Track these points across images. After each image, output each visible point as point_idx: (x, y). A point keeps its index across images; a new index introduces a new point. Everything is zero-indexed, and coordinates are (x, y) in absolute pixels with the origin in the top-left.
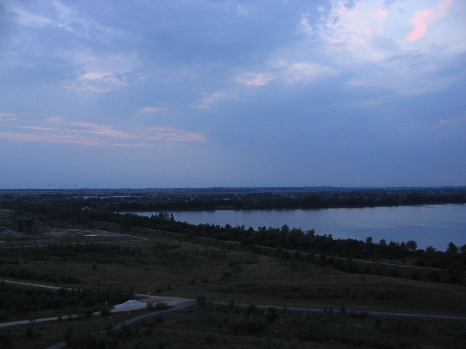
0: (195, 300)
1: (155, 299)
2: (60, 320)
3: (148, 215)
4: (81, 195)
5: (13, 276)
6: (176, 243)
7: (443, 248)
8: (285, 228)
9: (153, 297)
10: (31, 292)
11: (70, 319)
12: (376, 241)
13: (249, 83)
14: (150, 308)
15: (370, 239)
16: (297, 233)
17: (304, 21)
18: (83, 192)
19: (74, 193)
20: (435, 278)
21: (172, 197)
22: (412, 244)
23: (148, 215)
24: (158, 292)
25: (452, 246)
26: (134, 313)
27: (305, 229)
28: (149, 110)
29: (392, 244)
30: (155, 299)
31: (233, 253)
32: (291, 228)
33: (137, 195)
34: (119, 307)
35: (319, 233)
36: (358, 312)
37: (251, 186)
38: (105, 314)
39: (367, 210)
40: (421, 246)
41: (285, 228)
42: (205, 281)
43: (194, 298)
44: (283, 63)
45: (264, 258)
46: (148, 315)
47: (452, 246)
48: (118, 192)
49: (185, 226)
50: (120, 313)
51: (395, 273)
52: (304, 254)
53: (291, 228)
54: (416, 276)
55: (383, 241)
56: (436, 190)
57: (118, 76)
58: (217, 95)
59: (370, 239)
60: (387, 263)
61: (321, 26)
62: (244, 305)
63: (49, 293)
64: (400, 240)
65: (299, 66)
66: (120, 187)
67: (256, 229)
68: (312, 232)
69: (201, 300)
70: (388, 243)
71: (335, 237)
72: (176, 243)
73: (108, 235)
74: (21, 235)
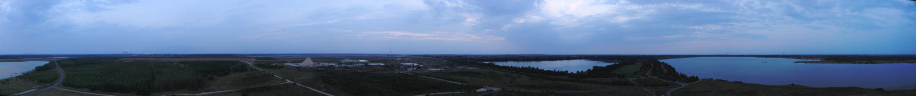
0: (468, 20)
1: (489, 88)
2: (461, 93)
3: (487, 63)
4: (395, 57)
5: (448, 80)
6: (496, 71)
7: (575, 72)
8: (529, 67)
9: (489, 88)
10: (454, 84)
11: (464, 93)
12: (556, 71)
13: (518, 22)
14: (488, 91)
15: (555, 70)
16: (533, 68)
17: (536, 3)
18: (468, 55)
19: (465, 55)
20: (573, 81)
21: (494, 57)
22: (567, 71)
23: (487, 63)
24: (490, 86)
25: (578, 72)
26: (483, 92)
27: (536, 67)
28: (487, 30)
29: (561, 71)
30: (489, 88)
31: (514, 75)
32: (531, 67)
33: (407, 58)
34: (478, 90)
35: (540, 68)
36: (551, 92)
37: (519, 54)
38: (474, 92)
39: (554, 62)
40: (569, 72)
41: (529, 67)
42: (504, 83)
43: (468, 22)
44: (529, 16)
45: (522, 76)
46: (486, 93)
47: (578, 72)
48: (478, 56)
49: (498, 66)
50: (479, 92)
51: (562, 80)
52: (535, 75)
53: (531, 67)
54: (568, 81)
55: (559, 71)
56: (574, 55)
57: (477, 20)
58: (509, 25)
59: (555, 70)
60: (560, 77)
61: (541, 5)
62: (517, 90)
63: (458, 85)
64: (564, 70)
65: (534, 17)
66: (479, 54)
67: (520, 67)
68: (538, 68)
69: (503, 89)
70: (560, 71)
71: (545, 70)
72: (496, 71)
73: (475, 68)
74: (449, 68)
